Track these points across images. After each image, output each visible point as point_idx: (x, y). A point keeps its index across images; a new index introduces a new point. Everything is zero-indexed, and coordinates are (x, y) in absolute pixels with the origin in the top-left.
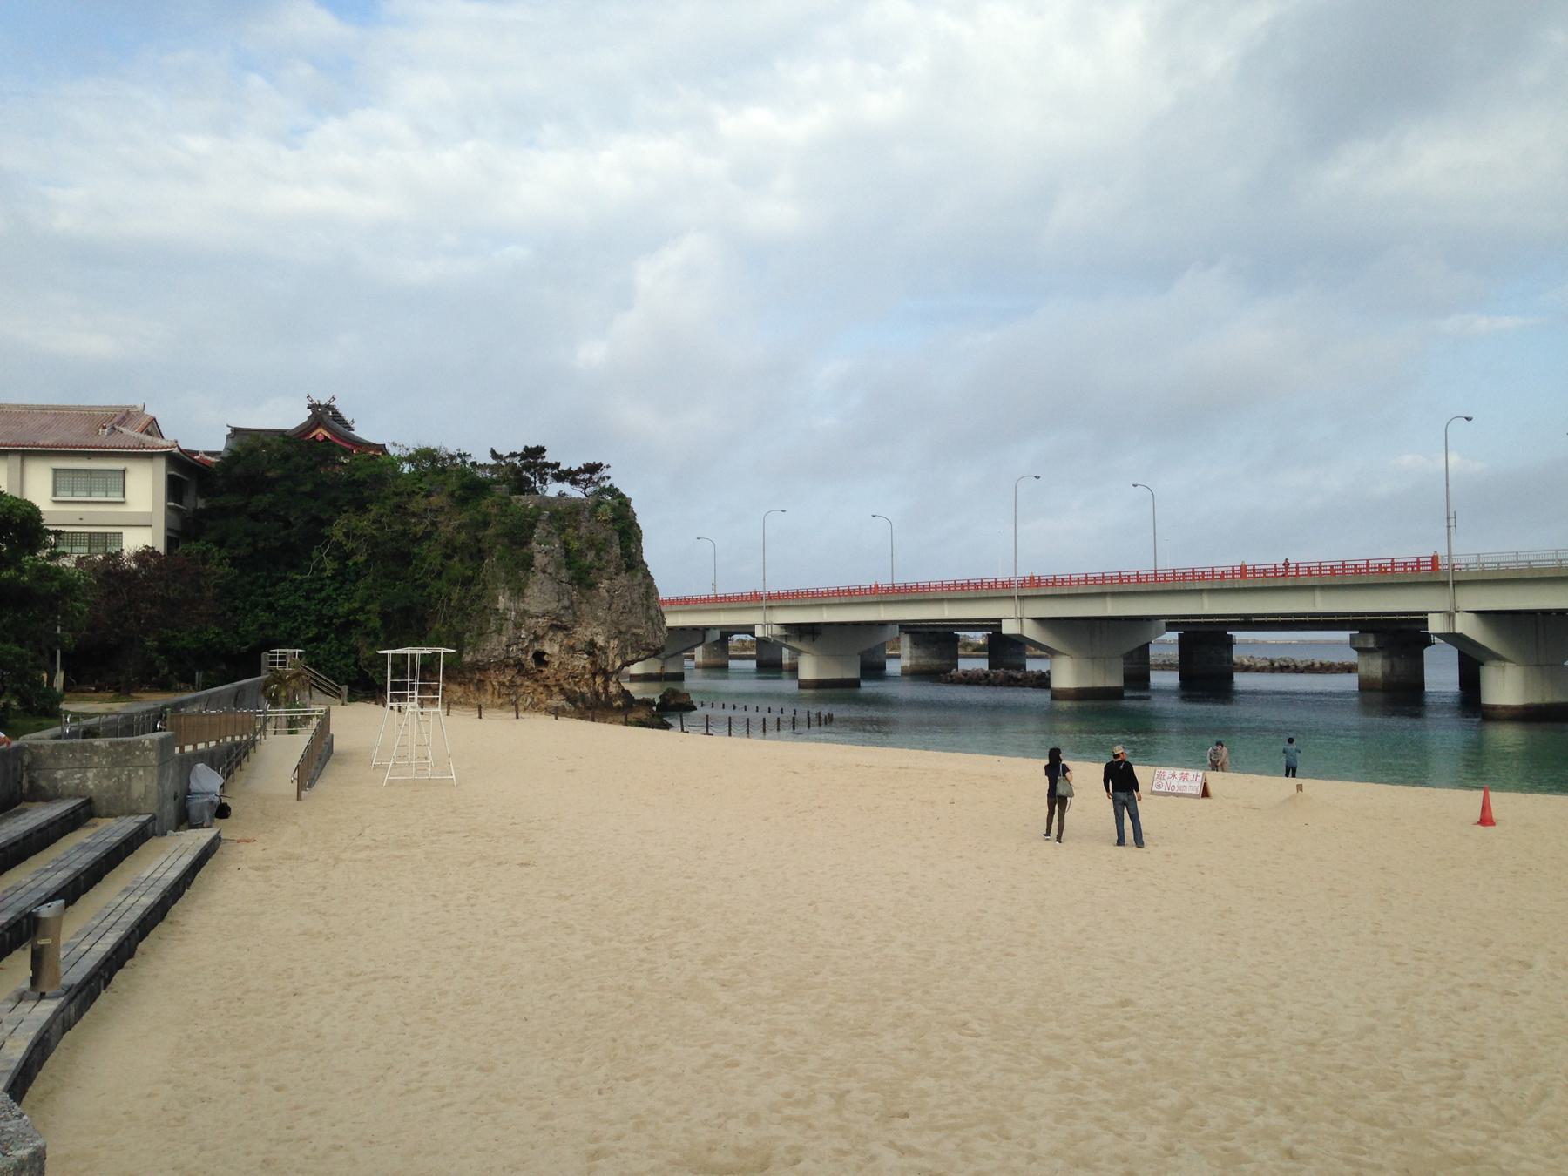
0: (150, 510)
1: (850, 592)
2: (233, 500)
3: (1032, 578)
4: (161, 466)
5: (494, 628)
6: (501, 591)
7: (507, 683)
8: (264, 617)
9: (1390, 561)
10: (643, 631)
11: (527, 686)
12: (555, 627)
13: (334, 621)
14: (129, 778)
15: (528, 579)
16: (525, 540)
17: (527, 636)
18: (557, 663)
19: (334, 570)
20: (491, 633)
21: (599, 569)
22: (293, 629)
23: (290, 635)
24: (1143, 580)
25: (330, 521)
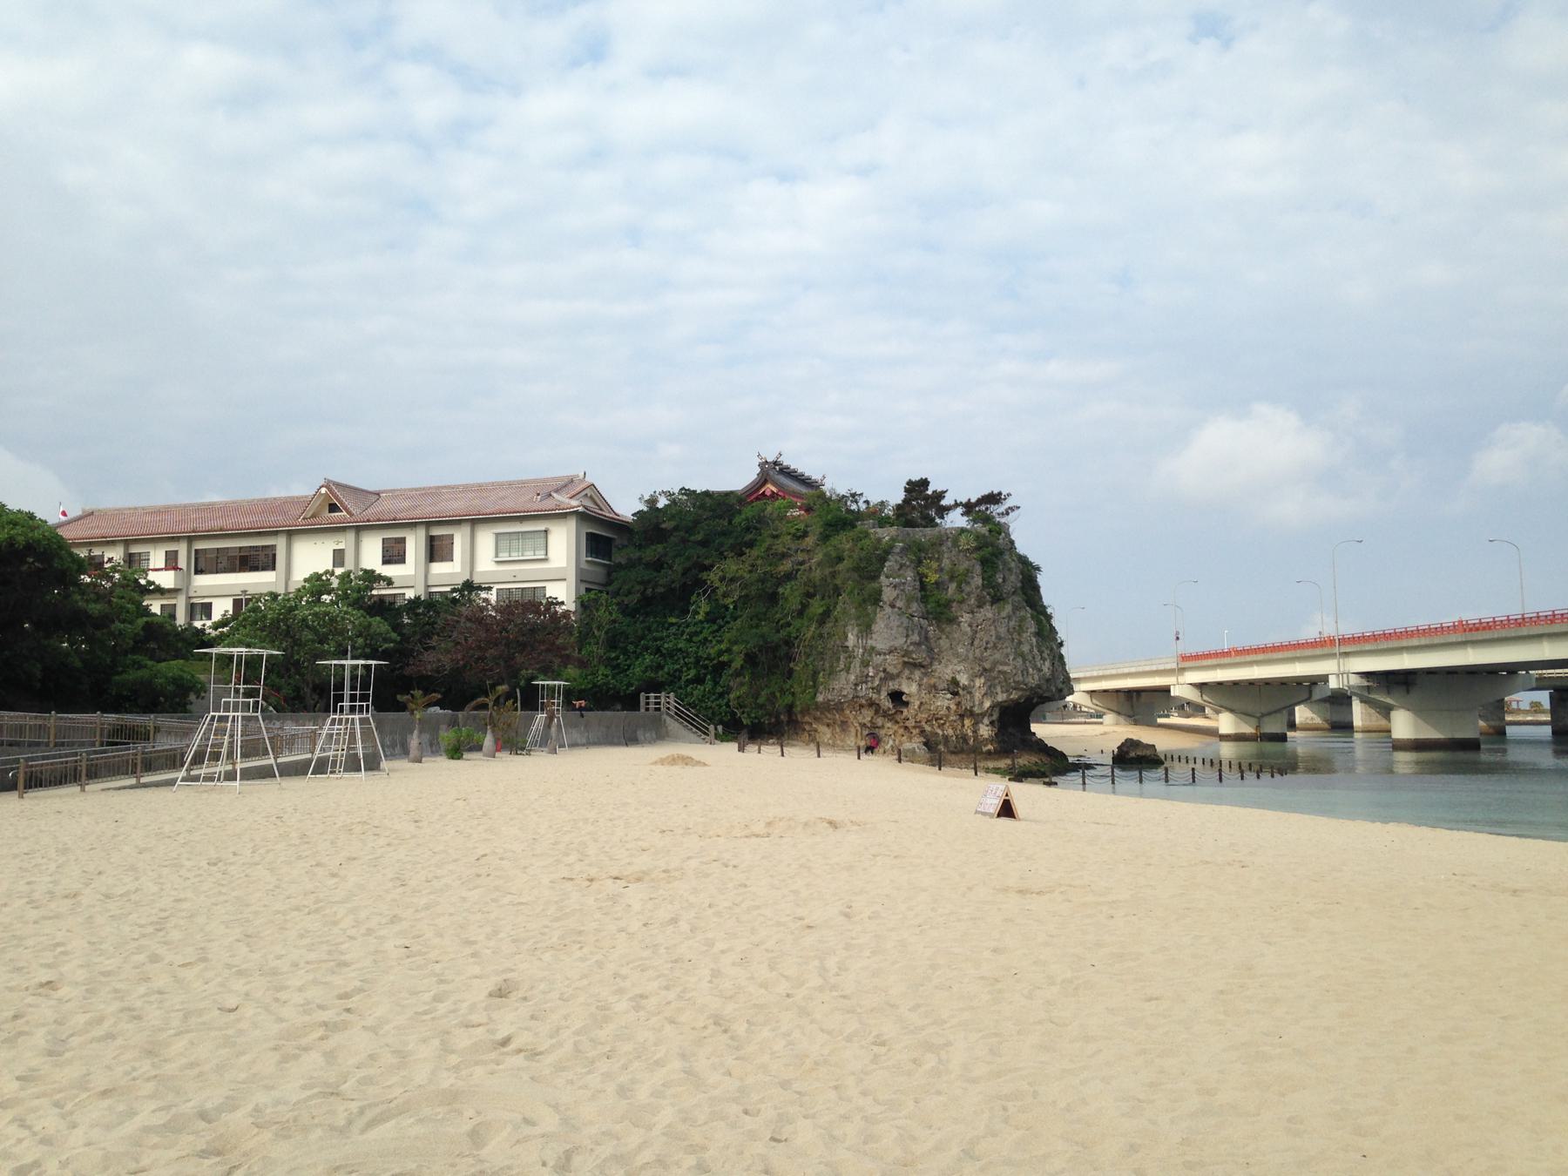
0: (565, 565)
4: (572, 524)
7: (869, 725)
10: (1010, 667)
11: (889, 728)
15: (876, 614)
18: (917, 703)
22: (676, 671)
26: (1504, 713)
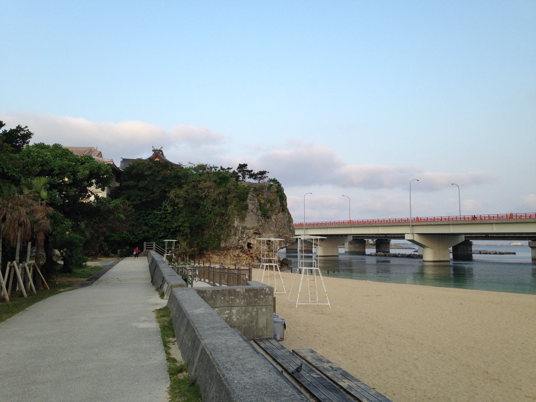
1: (322, 224)
2: (132, 183)
3: (417, 218)
5: (233, 233)
6: (236, 219)
7: (236, 255)
8: (145, 228)
9: (525, 214)
10: (288, 235)
11: (244, 257)
12: (255, 233)
13: (171, 230)
14: (257, 314)
15: (246, 214)
16: (245, 199)
17: (246, 237)
18: (255, 248)
19: (171, 210)
20: (232, 235)
21: (272, 211)
22: (155, 233)
23: (154, 235)
24: (406, 221)
25: (169, 192)
26: (388, 248)
